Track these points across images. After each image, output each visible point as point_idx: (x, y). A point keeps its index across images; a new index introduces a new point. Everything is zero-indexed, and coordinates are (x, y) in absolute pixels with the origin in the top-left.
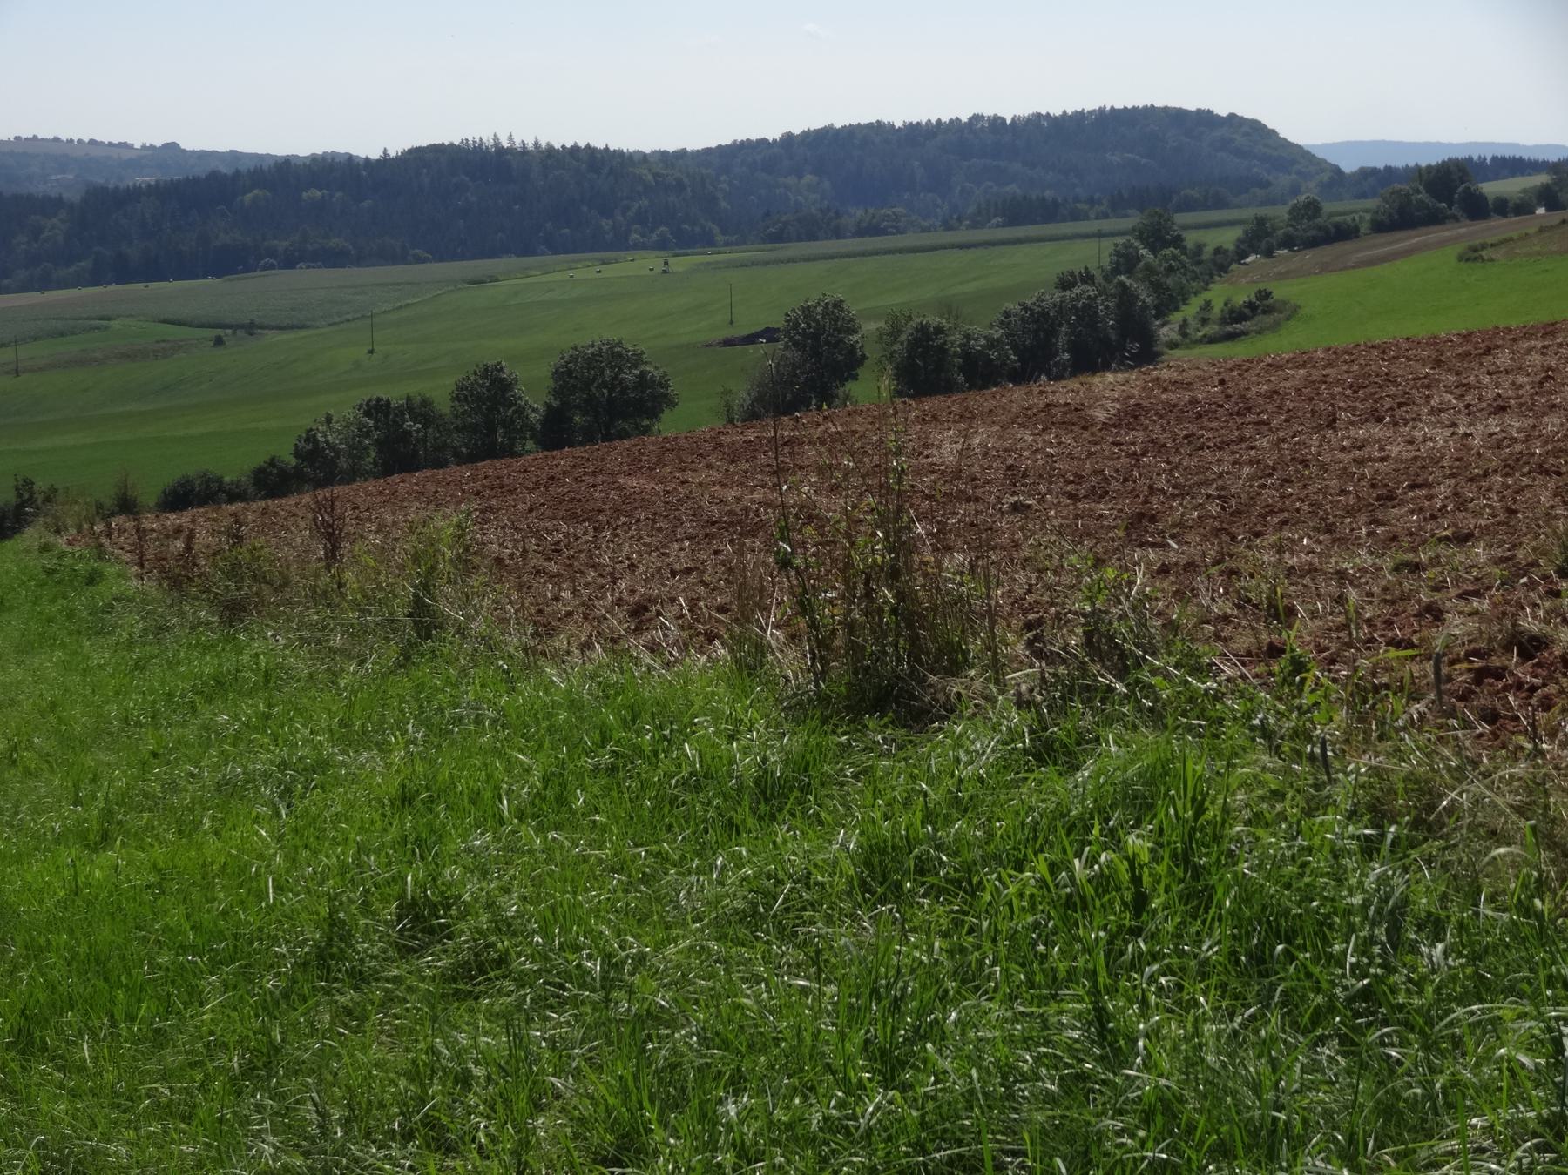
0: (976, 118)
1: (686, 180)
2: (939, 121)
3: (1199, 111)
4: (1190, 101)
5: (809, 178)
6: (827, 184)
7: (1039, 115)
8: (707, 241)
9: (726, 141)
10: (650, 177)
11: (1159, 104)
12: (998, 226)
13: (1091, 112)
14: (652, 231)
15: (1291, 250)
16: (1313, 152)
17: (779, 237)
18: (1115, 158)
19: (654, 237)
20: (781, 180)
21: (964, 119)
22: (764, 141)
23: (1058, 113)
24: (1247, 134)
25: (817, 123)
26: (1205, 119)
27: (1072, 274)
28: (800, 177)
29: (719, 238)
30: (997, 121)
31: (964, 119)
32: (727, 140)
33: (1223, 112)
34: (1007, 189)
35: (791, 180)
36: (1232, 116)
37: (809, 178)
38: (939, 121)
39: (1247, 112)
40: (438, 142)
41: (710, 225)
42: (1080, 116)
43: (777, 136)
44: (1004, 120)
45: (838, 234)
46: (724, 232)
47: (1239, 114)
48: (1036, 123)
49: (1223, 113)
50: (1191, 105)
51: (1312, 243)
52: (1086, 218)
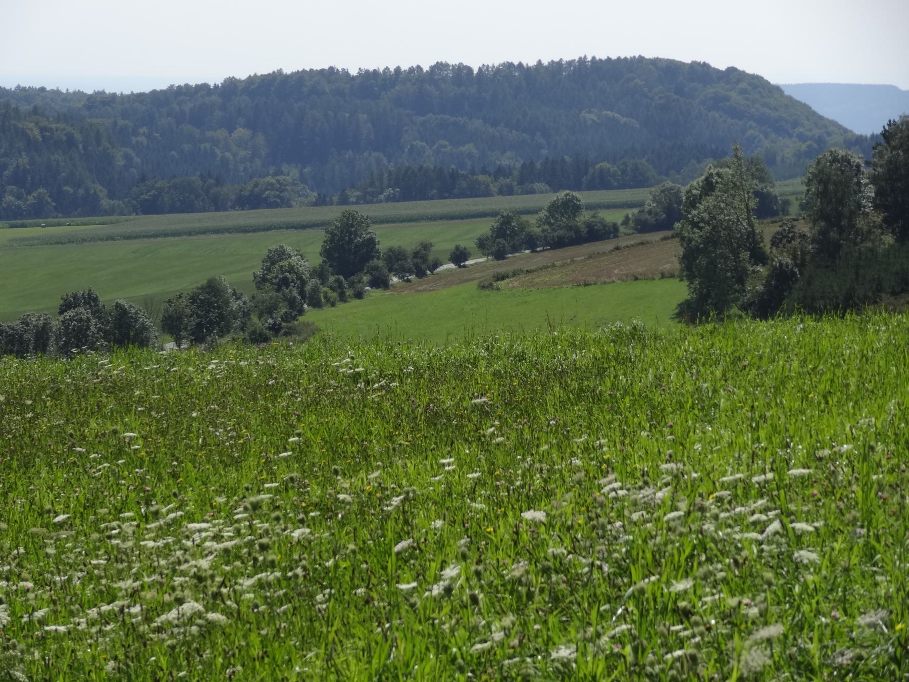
0: (439, 67)
1: (78, 136)
2: (398, 69)
3: (694, 64)
4: (684, 53)
5: (241, 132)
6: (260, 139)
7: (510, 65)
8: (89, 207)
9: (162, 86)
10: (36, 132)
11: (649, 55)
12: (388, 199)
13: (570, 63)
14: (29, 193)
15: (534, 251)
16: (827, 110)
17: (150, 207)
18: (590, 117)
19: (31, 199)
20: (209, 134)
21: (426, 68)
22: (205, 86)
23: (532, 63)
24: (743, 92)
25: (264, 69)
26: (700, 73)
27: (75, 296)
28: (231, 131)
29: (105, 203)
30: (462, 72)
31: (426, 68)
32: (162, 85)
33: (721, 64)
34: (463, 149)
35: (221, 134)
36: (732, 70)
37: (241, 132)
38: (398, 69)
39: (701, 59)
40: (142, 91)
41: (98, 187)
42: (557, 67)
43: (219, 81)
44: (470, 70)
45: (218, 204)
46: (112, 195)
47: (740, 68)
48: (510, 75)
49: (722, 67)
50: (685, 57)
51: (558, 244)
52: (487, 194)
